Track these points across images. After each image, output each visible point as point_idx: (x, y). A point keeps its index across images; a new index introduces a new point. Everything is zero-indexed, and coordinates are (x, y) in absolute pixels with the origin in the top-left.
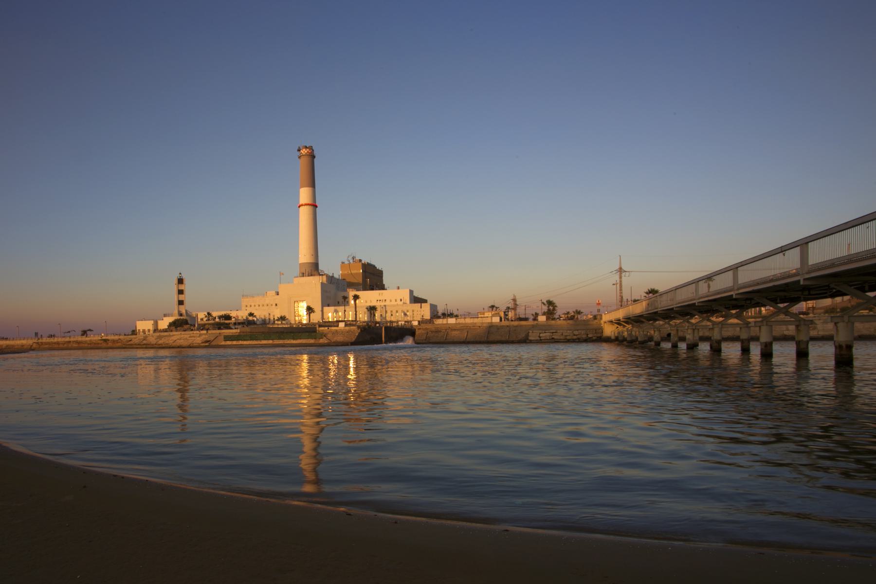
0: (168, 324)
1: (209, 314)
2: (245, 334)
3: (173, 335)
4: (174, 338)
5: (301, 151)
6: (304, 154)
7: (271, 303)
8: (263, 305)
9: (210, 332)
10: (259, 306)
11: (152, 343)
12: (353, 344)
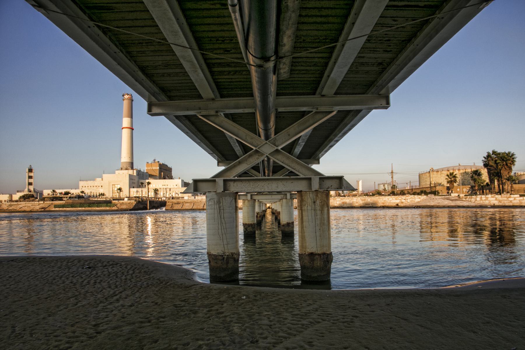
0: (19, 197)
1: (54, 191)
2: (69, 204)
3: (20, 204)
4: (21, 206)
5: (125, 96)
6: (126, 98)
7: (99, 185)
8: (93, 187)
9: (45, 202)
10: (91, 187)
11: (4, 209)
12: (131, 210)
